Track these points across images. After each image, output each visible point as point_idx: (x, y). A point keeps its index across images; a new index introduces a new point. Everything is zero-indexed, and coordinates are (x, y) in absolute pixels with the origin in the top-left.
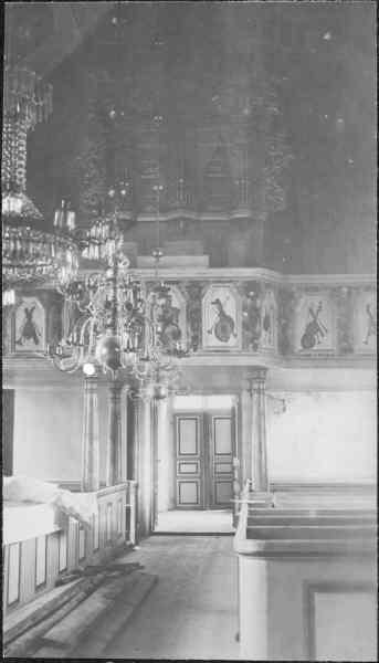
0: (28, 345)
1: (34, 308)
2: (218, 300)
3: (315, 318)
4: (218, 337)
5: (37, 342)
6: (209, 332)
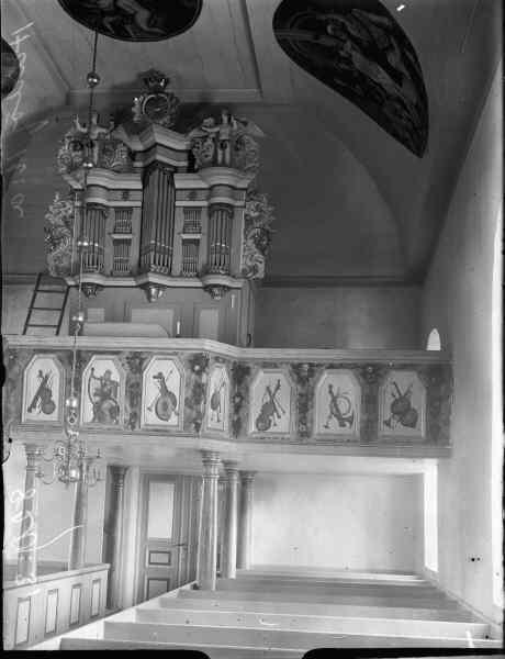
2: (160, 374)
3: (272, 396)
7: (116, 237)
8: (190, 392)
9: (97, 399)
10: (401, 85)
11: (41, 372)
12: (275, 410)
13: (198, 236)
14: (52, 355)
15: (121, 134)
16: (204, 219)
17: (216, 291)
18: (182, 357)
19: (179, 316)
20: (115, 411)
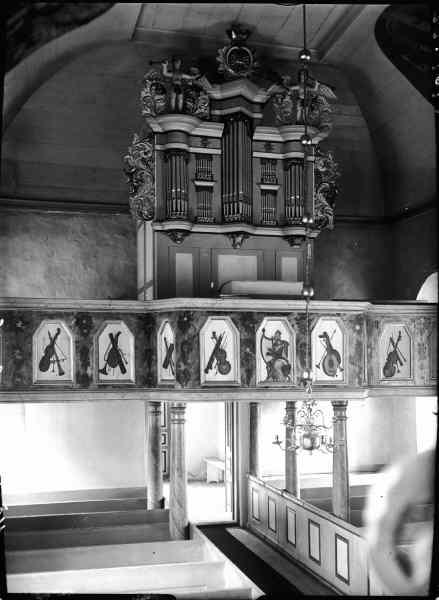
0: (114, 374)
1: (119, 333)
2: (325, 333)
3: (395, 346)
4: (325, 370)
5: (124, 371)
6: (318, 366)
7: (264, 187)
8: (354, 350)
9: (270, 358)
13: (275, 188)
14: (228, 317)
15: (205, 82)
16: (279, 170)
17: (298, 241)
18: (345, 318)
19: (262, 261)
20: (286, 369)
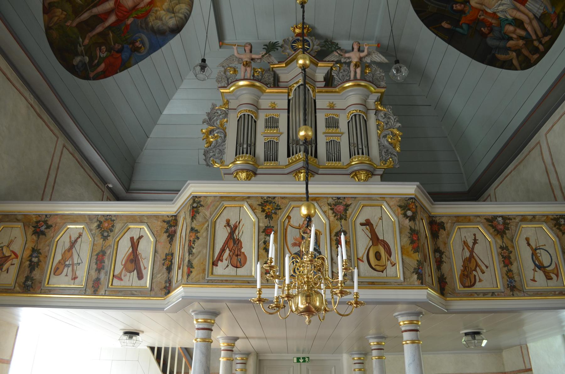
1: (140, 238)
3: (472, 251)
10: (485, 219)
11: (228, 222)
12: (477, 265)
